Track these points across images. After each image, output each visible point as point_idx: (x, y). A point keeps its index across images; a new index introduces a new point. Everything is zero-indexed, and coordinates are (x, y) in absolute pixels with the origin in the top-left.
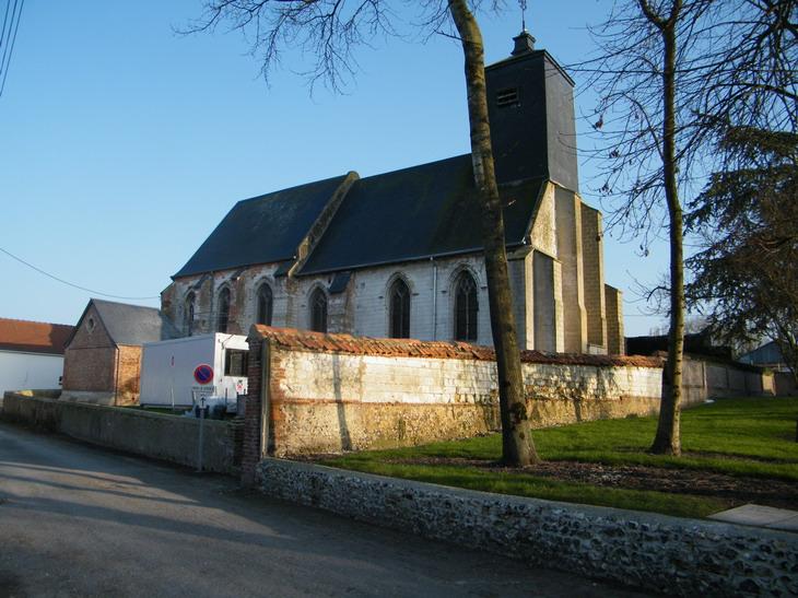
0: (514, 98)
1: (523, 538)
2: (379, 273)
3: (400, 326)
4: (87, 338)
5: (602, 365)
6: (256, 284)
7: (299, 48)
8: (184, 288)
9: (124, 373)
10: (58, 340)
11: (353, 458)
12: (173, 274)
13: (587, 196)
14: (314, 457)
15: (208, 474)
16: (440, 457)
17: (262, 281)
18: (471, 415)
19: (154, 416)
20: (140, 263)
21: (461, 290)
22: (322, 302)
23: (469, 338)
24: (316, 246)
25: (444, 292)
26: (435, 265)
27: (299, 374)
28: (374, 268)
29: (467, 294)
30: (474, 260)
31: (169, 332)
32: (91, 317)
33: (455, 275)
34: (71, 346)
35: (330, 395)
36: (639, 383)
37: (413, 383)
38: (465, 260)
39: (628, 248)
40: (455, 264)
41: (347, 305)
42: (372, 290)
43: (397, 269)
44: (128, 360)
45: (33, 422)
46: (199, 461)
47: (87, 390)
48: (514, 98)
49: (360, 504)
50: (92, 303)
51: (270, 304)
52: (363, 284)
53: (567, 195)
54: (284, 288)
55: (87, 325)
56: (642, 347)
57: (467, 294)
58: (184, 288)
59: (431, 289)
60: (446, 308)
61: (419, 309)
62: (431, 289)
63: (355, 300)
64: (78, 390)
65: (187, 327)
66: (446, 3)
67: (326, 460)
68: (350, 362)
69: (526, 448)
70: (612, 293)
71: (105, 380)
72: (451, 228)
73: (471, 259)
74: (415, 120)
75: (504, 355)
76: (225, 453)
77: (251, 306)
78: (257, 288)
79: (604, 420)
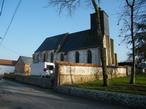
0: (98, 19)
1: (115, 85)
3: (77, 61)
4: (20, 63)
5: (116, 67)
7: (65, 10)
9: (26, 69)
10: (14, 63)
11: (74, 85)
13: (111, 37)
14: (66, 85)
15: (47, 88)
16: (90, 84)
18: (93, 77)
19: (32, 77)
20: (29, 50)
24: (61, 46)
27: (64, 70)
31: (34, 62)
35: (108, 70)
36: (122, 71)
37: (83, 71)
39: (121, 48)
42: (72, 54)
44: (27, 67)
45: (9, 78)
46: (44, 85)
48: (98, 19)
49: (74, 92)
53: (108, 37)
56: (122, 64)
59: (83, 54)
60: (86, 58)
61: (81, 58)
62: (83, 54)
65: (101, 70)
68: (73, 68)
69: (108, 83)
70: (112, 40)
71: (23, 71)
72: (91, 40)
74: (82, 24)
75: (103, 67)
76: (51, 84)
77: (49, 57)
79: (116, 78)
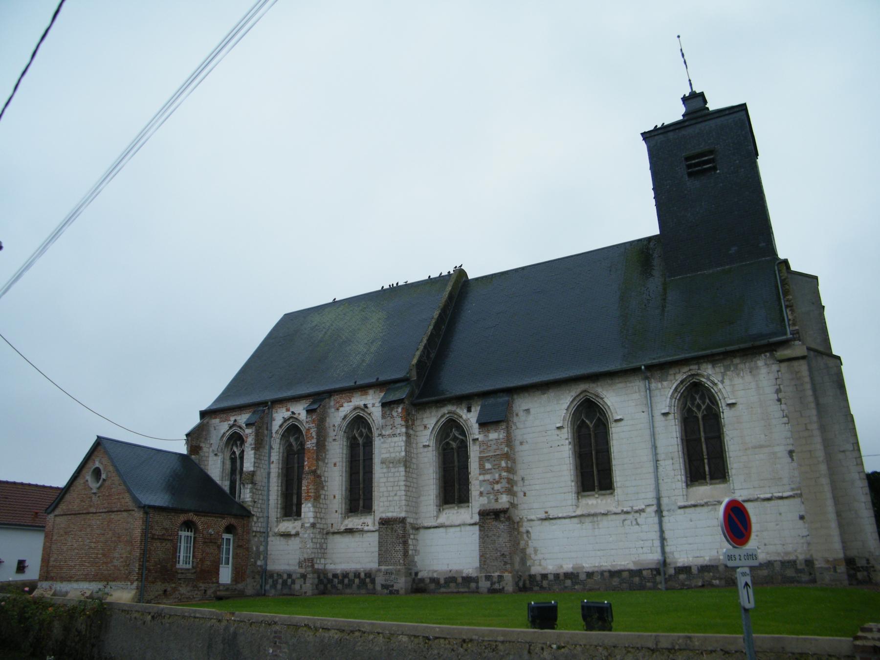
2: (551, 394)
6: (345, 417)
8: (221, 427)
12: (203, 408)
17: (354, 414)
21: (690, 411)
22: (455, 439)
23: (712, 478)
25: (665, 414)
26: (647, 378)
28: (544, 387)
29: (700, 416)
30: (710, 366)
32: (97, 464)
33: (682, 389)
34: (57, 512)
38: (696, 367)
40: (678, 377)
41: (509, 441)
43: (582, 387)
47: (87, 578)
50: (100, 444)
51: (369, 443)
52: (527, 411)
54: (399, 421)
55: (88, 476)
57: (700, 416)
58: (221, 427)
60: (670, 436)
63: (518, 434)
64: (69, 579)
66: (878, 470)
67: (721, 357)
73: (704, 366)
78: (345, 424)
